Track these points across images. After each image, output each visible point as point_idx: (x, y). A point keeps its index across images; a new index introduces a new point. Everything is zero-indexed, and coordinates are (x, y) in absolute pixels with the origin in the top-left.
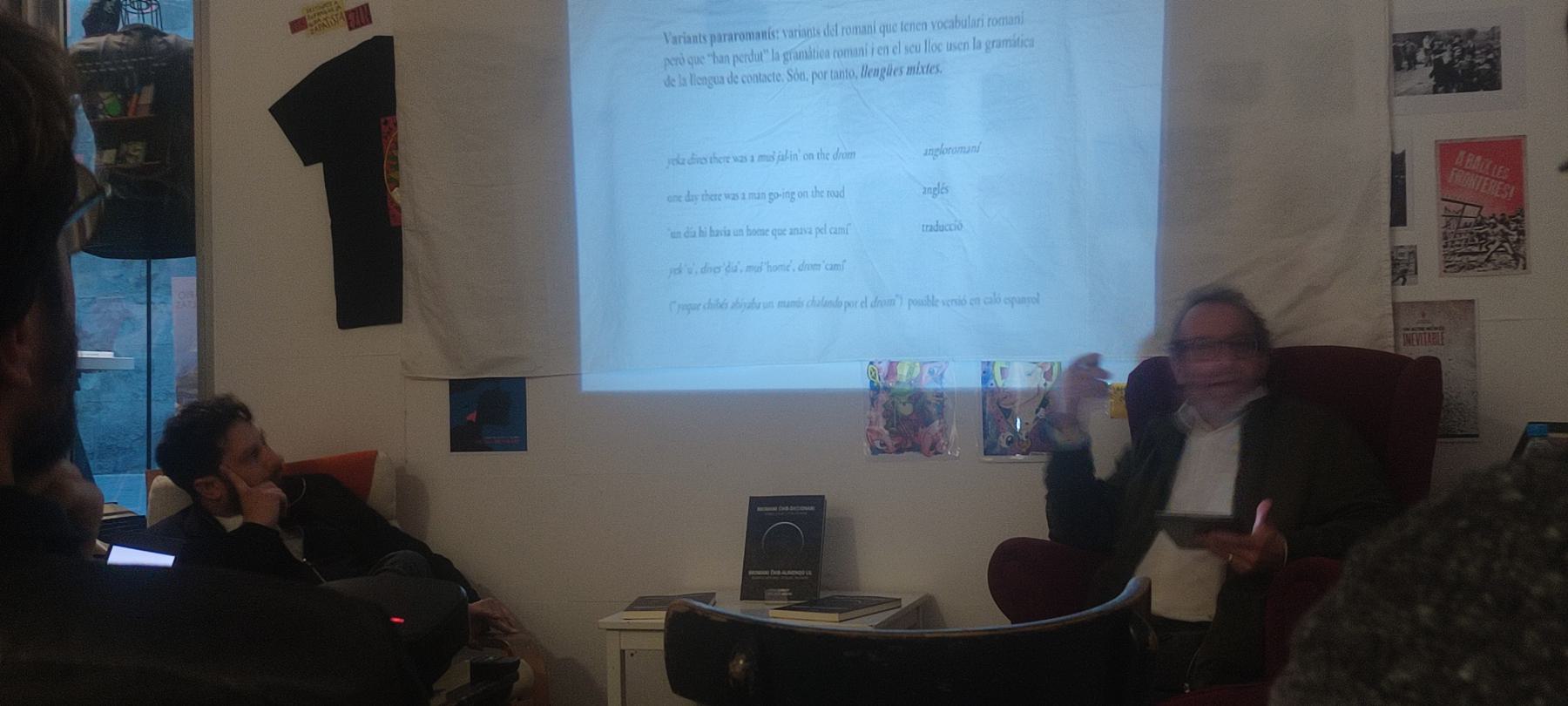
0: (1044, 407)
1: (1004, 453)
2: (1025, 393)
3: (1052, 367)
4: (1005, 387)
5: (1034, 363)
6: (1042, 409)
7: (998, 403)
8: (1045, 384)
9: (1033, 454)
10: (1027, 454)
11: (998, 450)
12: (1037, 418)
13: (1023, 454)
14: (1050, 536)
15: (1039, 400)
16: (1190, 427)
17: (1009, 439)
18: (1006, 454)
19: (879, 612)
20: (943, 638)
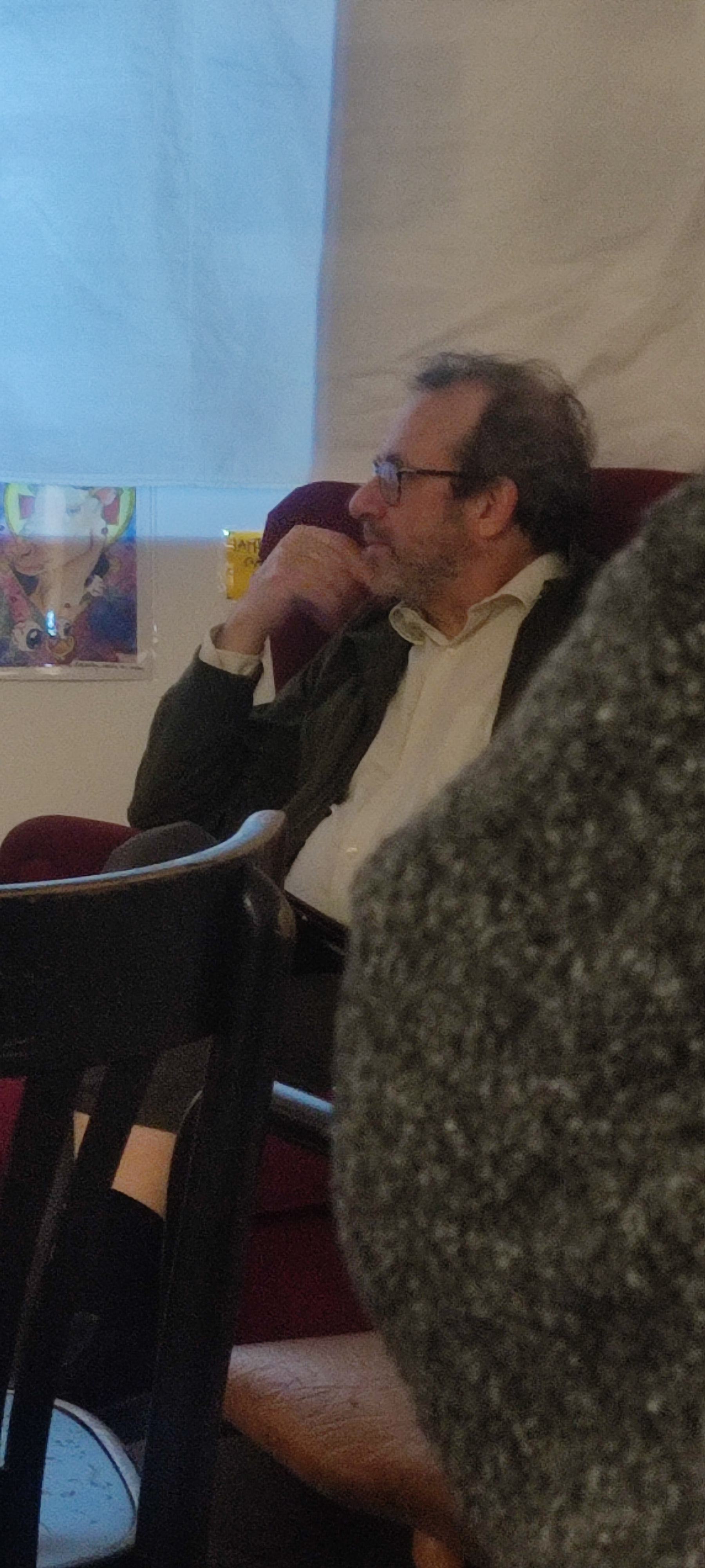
1: (22, 661)
2: (69, 545)
3: (117, 499)
4: (28, 533)
5: (85, 488)
6: (97, 578)
7: (13, 567)
8: (105, 531)
9: (76, 665)
10: (67, 662)
11: (10, 655)
13: (60, 663)
14: (130, 818)
15: (94, 559)
16: (8, 637)
17: (34, 635)
18: (24, 665)
20: (15, 899)
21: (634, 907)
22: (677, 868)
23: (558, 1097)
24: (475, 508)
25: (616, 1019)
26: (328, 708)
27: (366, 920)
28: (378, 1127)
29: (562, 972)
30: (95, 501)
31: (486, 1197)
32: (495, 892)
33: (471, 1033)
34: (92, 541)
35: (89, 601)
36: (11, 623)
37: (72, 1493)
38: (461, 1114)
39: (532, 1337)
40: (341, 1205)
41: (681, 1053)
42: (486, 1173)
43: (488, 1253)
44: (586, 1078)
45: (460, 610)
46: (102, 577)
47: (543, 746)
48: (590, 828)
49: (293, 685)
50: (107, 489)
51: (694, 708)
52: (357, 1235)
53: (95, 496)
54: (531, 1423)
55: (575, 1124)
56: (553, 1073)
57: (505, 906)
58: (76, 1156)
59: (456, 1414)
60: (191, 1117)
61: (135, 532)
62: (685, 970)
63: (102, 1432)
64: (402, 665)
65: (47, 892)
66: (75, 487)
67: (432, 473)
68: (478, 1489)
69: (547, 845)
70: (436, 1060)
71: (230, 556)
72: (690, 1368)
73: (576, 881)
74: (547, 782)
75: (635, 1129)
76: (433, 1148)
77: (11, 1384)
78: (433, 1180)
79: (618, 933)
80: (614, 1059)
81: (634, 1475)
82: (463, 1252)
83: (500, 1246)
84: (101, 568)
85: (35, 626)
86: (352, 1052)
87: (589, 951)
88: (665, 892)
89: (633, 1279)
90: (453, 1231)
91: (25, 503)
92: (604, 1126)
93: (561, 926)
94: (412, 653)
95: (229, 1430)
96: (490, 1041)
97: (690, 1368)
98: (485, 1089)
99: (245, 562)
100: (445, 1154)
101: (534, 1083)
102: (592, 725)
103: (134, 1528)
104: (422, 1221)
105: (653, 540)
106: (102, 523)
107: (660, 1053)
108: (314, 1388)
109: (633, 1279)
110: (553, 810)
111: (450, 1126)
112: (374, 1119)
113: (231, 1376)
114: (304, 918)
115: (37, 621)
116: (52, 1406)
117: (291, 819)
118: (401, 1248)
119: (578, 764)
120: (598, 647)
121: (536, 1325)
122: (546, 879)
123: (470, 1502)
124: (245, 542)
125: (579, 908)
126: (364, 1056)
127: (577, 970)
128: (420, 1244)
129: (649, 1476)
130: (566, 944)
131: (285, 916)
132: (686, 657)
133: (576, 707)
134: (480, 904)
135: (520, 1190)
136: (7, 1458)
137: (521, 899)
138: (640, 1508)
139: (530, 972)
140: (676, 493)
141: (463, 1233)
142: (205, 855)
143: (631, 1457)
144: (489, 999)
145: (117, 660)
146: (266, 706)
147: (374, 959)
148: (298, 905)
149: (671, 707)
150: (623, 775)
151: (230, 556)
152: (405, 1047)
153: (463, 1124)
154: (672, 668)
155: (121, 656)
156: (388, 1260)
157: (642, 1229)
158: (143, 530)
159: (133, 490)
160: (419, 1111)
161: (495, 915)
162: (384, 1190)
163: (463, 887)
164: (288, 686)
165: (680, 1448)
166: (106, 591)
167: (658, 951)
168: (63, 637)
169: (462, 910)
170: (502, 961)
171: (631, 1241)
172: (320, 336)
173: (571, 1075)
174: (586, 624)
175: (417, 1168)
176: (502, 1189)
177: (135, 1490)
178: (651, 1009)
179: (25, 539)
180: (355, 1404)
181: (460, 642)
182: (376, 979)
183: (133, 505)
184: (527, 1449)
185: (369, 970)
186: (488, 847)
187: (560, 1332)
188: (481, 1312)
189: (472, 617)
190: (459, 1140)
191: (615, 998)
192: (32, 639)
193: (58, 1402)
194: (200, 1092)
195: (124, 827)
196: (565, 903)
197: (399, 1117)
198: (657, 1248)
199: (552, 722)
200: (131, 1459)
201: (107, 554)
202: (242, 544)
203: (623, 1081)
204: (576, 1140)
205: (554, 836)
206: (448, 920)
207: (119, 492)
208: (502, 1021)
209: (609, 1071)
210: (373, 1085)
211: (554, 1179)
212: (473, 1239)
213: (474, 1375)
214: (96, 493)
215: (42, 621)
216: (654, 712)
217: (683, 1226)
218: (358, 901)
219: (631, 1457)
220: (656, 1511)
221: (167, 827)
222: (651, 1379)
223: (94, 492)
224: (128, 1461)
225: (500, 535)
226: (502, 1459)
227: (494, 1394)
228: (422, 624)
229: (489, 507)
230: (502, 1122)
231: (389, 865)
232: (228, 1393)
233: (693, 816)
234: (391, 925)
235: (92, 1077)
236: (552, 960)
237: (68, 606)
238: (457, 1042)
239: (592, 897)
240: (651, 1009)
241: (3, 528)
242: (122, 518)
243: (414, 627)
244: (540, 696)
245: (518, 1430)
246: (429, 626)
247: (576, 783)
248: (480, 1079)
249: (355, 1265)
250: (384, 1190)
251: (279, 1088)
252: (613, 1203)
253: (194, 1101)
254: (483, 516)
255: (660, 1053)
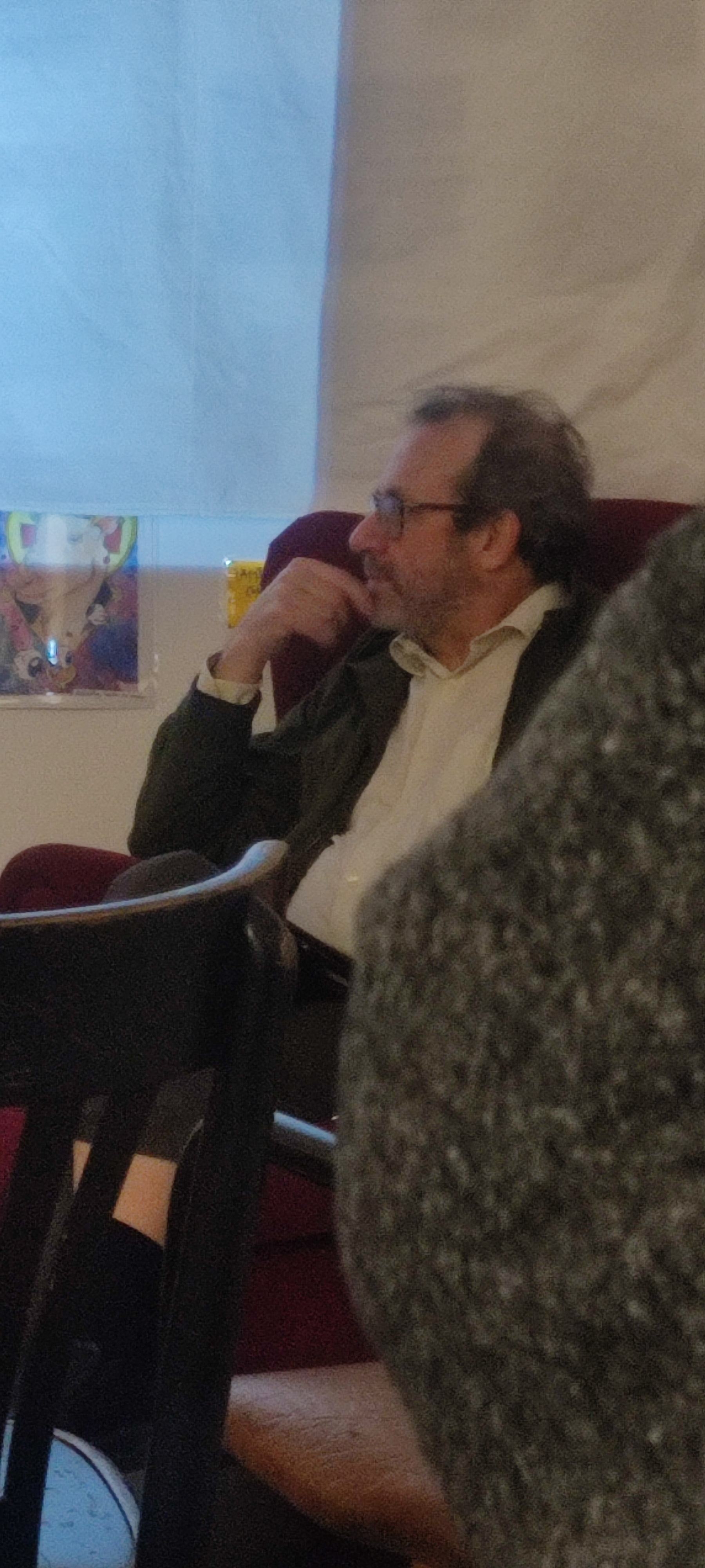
0: (101, 603)
1: (23, 689)
3: (119, 529)
4: (29, 562)
5: (87, 517)
6: (99, 608)
7: (14, 594)
8: (107, 560)
9: (77, 694)
11: (11, 683)
12: (90, 625)
13: (60, 691)
15: (94, 590)
17: (35, 664)
19: (120, 1506)
21: (637, 937)
22: (682, 898)
23: (561, 1127)
24: (478, 540)
25: (619, 1049)
26: (327, 739)
27: (370, 949)
28: (382, 1156)
29: (566, 1003)
30: (97, 531)
31: (489, 1225)
32: (500, 920)
33: (475, 1062)
34: (94, 570)
35: (91, 630)
36: (12, 651)
37: (72, 1524)
38: (464, 1144)
39: (534, 1367)
40: (344, 1232)
41: (685, 1085)
42: (489, 1200)
43: (491, 1282)
44: (589, 1108)
45: (462, 641)
46: (104, 606)
47: (548, 776)
48: (595, 858)
49: (294, 714)
50: (108, 518)
51: (698, 740)
52: (359, 1262)
53: (97, 525)
54: (532, 1450)
55: (578, 1154)
56: (557, 1102)
57: (510, 934)
58: (76, 1186)
59: (459, 1441)
60: (194, 1142)
61: (136, 561)
62: (690, 1001)
63: (101, 1463)
64: (403, 695)
65: (49, 921)
66: (77, 516)
67: (435, 507)
68: (479, 1515)
69: (551, 874)
70: (440, 1088)
71: (231, 585)
72: (691, 1399)
73: (582, 909)
74: (552, 812)
75: (639, 1159)
76: (436, 1173)
77: (11, 1413)
78: (435, 1208)
79: (623, 962)
80: (618, 1090)
81: (636, 1506)
82: (466, 1279)
83: (503, 1274)
84: (103, 596)
85: (37, 654)
86: (355, 1079)
87: (593, 984)
88: (670, 924)
89: (635, 1309)
90: (456, 1258)
91: (27, 532)
92: (607, 1157)
93: (564, 957)
94: (413, 684)
95: (228, 1460)
96: (494, 1071)
97: (691, 1399)
98: (488, 1118)
99: (247, 592)
100: (448, 1182)
101: (537, 1113)
102: (596, 754)
103: (133, 1561)
104: (425, 1248)
105: (659, 573)
106: (103, 552)
107: (664, 1084)
108: (314, 1419)
109: (635, 1309)
110: (557, 841)
111: (453, 1154)
112: (378, 1147)
113: (231, 1407)
114: (305, 947)
115: (36, 649)
116: (50, 1436)
117: (292, 850)
118: (404, 1275)
119: (583, 796)
120: (604, 678)
121: (539, 1354)
122: (551, 909)
123: (472, 1529)
124: (247, 572)
125: (583, 938)
126: (367, 1082)
127: (581, 999)
128: (422, 1270)
129: (651, 1506)
130: (569, 974)
131: (287, 946)
132: (691, 688)
133: (580, 740)
134: (484, 933)
135: (523, 1221)
136: (8, 1488)
137: (525, 930)
138: (642, 1537)
139: (533, 1001)
140: (682, 524)
141: (465, 1259)
142: (205, 885)
143: (633, 1488)
144: (491, 1026)
145: (117, 688)
146: (266, 736)
147: (378, 986)
148: (300, 935)
149: (675, 738)
150: (629, 806)
151: (231, 585)
152: (408, 1075)
153: (467, 1154)
154: (678, 700)
155: (122, 684)
156: (390, 1287)
157: (644, 1256)
158: (145, 559)
159: (135, 520)
160: (422, 1139)
161: (499, 944)
162: (387, 1217)
163: (468, 916)
164: (287, 717)
165: (682, 1479)
166: (108, 619)
167: (662, 982)
168: (64, 665)
169: (468, 936)
170: (505, 989)
171: (633, 1272)
172: (322, 365)
173: (576, 1106)
174: (591, 654)
175: (420, 1196)
176: (505, 1218)
177: (134, 1521)
178: (656, 1040)
179: (28, 568)
180: (354, 1435)
181: (461, 673)
182: (380, 1008)
183: (135, 534)
184: (526, 1476)
185: (372, 998)
186: (493, 877)
187: (562, 1362)
188: (483, 1339)
189: (474, 648)
190: (462, 1169)
191: (618, 1028)
192: (34, 668)
193: (58, 1433)
194: (201, 1121)
195: (126, 856)
196: (568, 933)
197: (402, 1145)
198: (659, 1279)
199: (558, 753)
200: (131, 1489)
201: (109, 583)
202: (244, 573)
203: (627, 1111)
204: (578, 1169)
205: (558, 866)
206: (452, 947)
207: (120, 521)
208: (505, 1050)
209: (612, 1101)
210: (376, 1112)
211: (556, 1207)
212: (475, 1266)
213: (475, 1402)
214: (98, 522)
215: (43, 649)
216: (658, 743)
217: (684, 1256)
218: (363, 928)
219: (633, 1488)
220: (659, 1542)
221: (167, 856)
222: (651, 1408)
223: (96, 521)
224: (126, 1491)
225: (500, 568)
226: (504, 1487)
227: (496, 1421)
228: (423, 655)
229: (491, 539)
230: (504, 1149)
231: (394, 891)
232: (228, 1421)
233: (697, 847)
234: (396, 953)
235: (92, 1107)
236: (556, 990)
237: (69, 634)
238: (460, 1071)
239: (596, 928)
240: (656, 1040)
241: (4, 557)
242: (124, 546)
243: (415, 658)
244: (545, 726)
245: (519, 1461)
246: (432, 659)
247: (581, 814)
248: (482, 1107)
249: (358, 1292)
250: (387, 1217)
251: (281, 1118)
252: (616, 1233)
253: (195, 1129)
254: (486, 548)
255: (664, 1084)
